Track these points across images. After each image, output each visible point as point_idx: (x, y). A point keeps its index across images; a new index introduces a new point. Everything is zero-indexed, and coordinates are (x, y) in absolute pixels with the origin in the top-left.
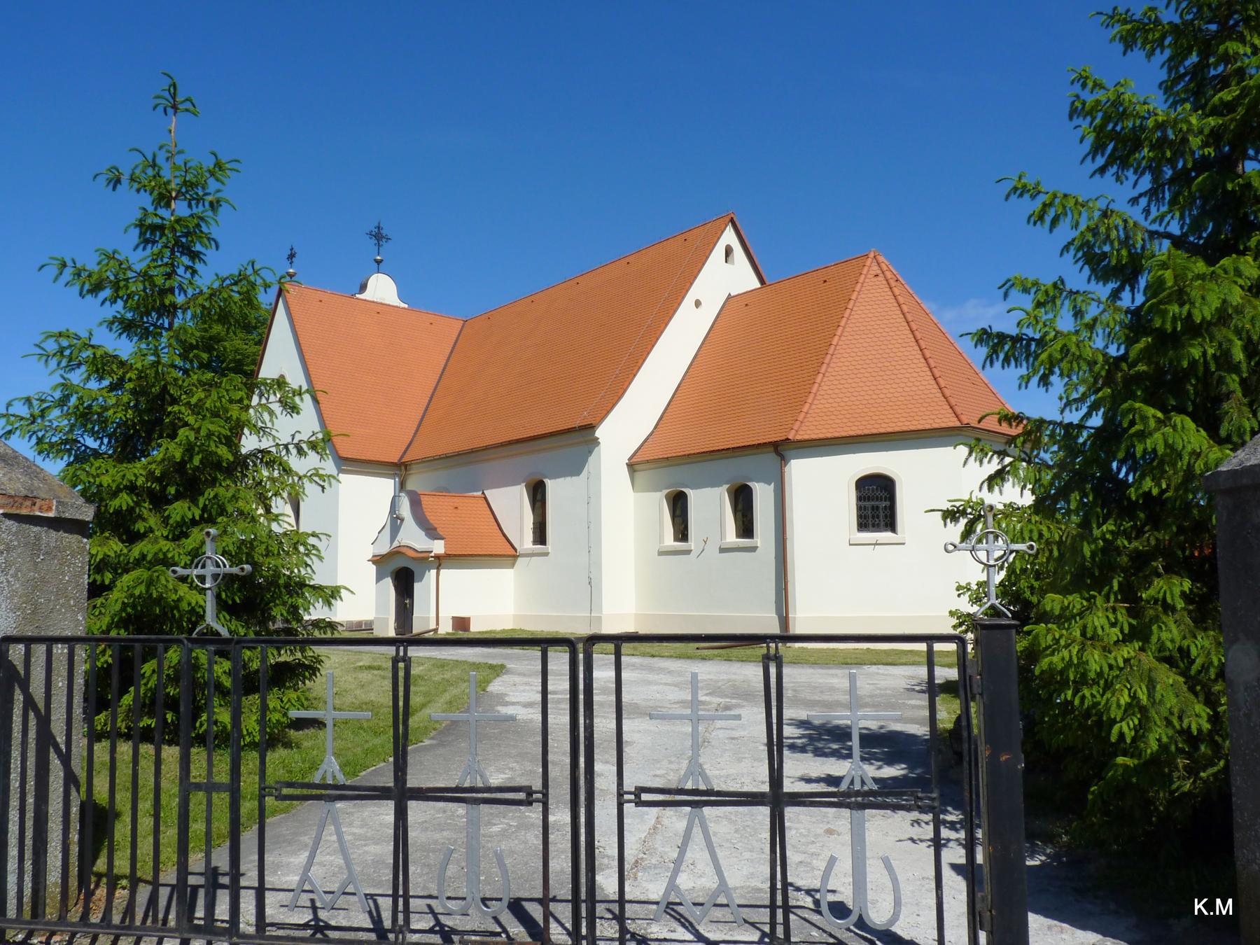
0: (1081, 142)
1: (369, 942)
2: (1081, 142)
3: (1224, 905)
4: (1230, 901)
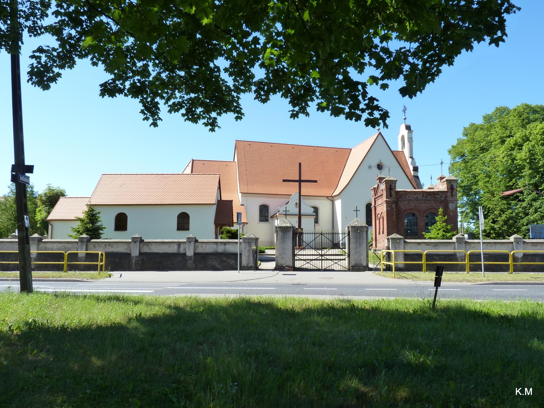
1: (17, 264)
4: (531, 389)
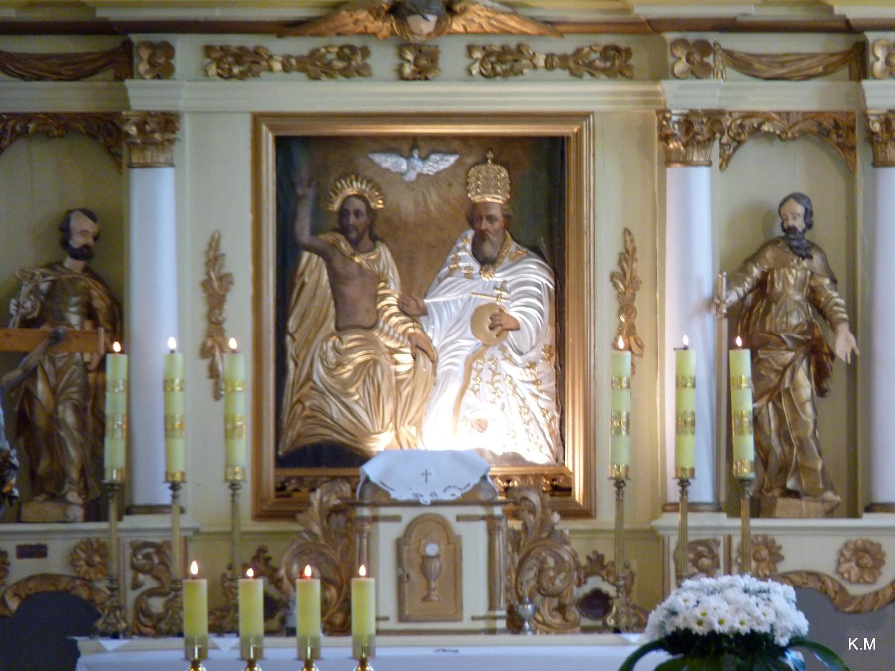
0: (502, 409)
2: (502, 409)
3: (870, 642)
4: (874, 640)
